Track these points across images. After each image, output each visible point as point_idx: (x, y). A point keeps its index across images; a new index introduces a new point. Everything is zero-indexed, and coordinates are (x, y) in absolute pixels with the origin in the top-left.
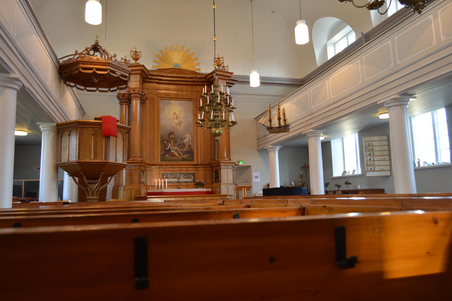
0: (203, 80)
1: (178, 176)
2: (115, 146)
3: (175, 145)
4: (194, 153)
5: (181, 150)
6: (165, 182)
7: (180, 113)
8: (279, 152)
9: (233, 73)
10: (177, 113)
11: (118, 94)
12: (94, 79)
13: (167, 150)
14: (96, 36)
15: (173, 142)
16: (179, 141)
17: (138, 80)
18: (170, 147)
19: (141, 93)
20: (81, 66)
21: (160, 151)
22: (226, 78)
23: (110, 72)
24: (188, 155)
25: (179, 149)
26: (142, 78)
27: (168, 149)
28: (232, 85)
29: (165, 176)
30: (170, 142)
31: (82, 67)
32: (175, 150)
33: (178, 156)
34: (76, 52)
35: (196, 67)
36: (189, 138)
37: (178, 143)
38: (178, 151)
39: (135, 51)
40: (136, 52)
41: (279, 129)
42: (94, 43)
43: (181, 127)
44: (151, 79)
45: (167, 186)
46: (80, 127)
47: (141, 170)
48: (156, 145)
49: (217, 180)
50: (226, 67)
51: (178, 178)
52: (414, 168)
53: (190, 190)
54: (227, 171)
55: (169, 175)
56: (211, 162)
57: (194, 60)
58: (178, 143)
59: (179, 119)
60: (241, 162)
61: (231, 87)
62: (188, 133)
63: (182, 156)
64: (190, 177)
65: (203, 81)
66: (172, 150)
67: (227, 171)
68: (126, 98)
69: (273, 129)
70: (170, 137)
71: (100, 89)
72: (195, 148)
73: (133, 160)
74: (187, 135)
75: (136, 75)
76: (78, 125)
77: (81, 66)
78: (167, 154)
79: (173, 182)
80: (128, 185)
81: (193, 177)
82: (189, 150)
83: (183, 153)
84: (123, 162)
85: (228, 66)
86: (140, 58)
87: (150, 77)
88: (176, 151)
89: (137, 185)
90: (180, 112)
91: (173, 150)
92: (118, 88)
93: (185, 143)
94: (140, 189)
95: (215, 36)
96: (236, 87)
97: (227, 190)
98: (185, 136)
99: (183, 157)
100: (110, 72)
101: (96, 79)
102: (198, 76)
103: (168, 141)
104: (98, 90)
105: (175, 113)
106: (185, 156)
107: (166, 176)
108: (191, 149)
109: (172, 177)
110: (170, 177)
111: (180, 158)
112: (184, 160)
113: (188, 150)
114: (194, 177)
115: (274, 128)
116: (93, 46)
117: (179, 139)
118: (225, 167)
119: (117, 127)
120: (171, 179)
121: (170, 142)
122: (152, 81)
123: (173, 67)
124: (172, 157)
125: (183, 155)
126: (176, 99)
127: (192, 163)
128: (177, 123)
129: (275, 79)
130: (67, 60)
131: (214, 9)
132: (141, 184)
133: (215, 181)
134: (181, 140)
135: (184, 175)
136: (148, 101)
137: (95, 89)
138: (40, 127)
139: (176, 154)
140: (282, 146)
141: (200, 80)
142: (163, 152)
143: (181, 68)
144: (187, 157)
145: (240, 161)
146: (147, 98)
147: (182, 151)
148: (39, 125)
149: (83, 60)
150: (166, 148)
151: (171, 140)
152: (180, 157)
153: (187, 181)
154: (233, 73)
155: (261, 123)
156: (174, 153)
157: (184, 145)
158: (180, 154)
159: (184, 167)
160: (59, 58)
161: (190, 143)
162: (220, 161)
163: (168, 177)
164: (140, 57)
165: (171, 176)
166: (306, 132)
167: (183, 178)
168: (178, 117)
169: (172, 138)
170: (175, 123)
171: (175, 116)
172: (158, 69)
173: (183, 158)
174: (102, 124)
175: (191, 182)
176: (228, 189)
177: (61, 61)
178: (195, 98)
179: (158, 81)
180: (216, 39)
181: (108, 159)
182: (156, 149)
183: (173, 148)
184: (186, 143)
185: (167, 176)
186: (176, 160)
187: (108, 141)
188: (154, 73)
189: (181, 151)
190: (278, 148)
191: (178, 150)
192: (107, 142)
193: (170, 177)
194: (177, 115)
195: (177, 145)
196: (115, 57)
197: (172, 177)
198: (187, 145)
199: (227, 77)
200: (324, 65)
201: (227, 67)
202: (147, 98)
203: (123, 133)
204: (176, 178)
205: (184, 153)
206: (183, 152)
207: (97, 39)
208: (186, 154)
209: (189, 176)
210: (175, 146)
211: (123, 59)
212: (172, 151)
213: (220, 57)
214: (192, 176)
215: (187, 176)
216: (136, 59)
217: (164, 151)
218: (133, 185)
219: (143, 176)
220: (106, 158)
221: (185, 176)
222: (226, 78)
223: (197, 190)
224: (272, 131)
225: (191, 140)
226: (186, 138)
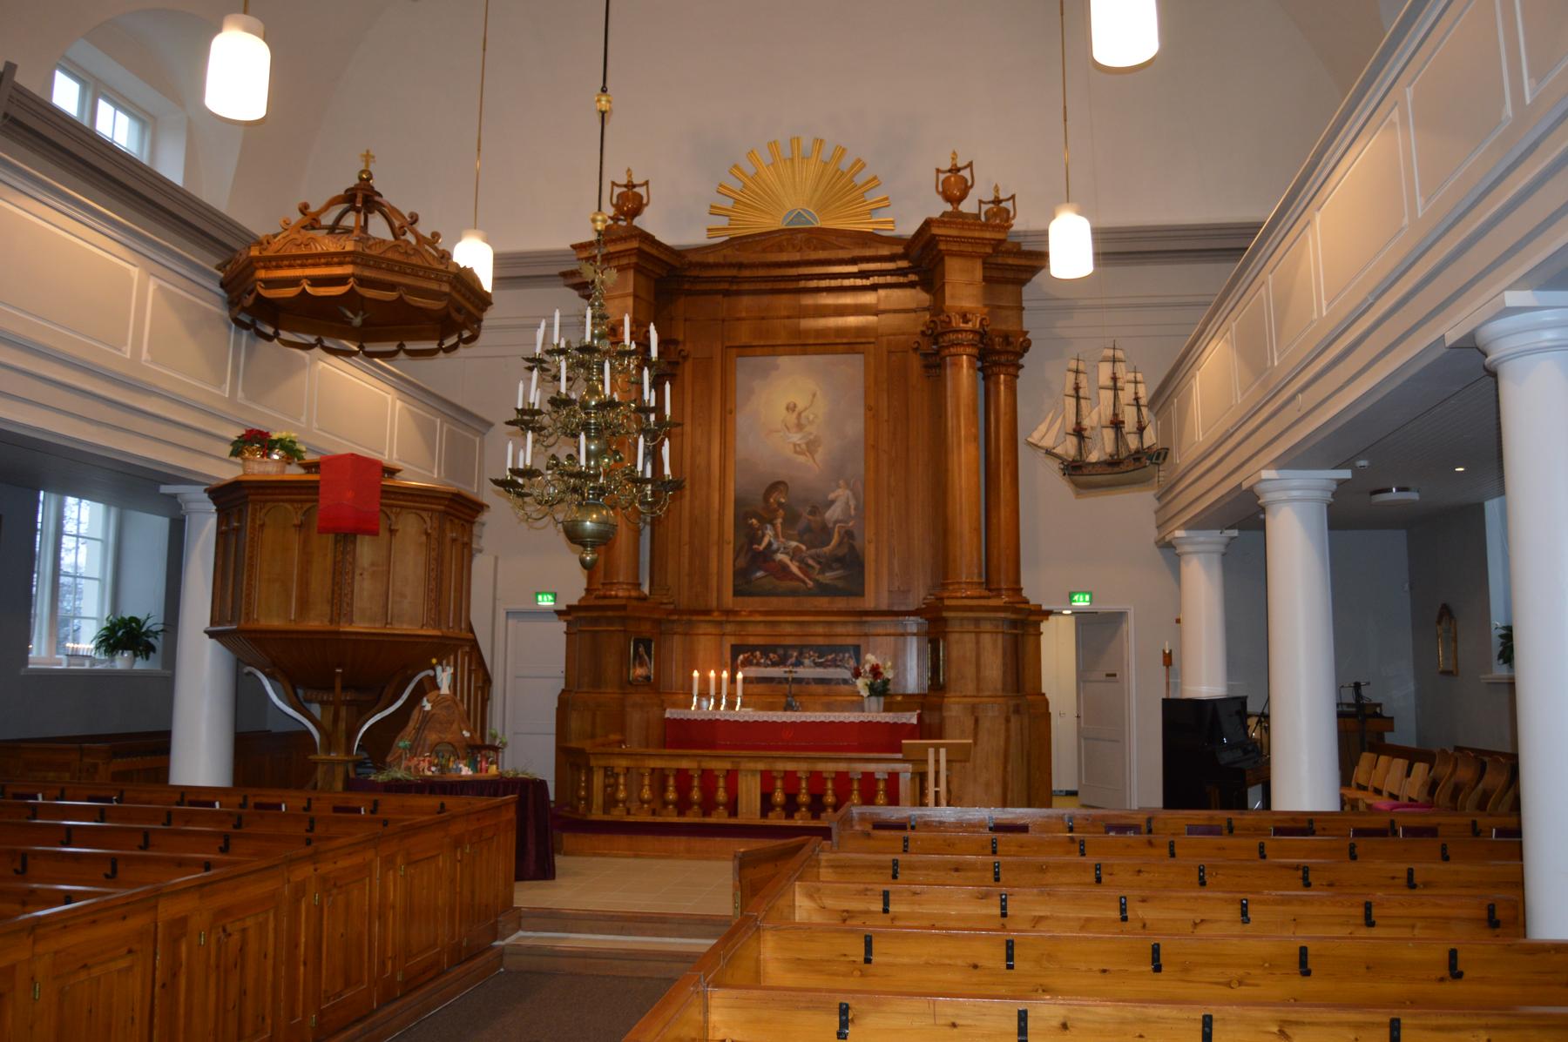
1: (791, 657)
3: (791, 532)
5: (813, 551)
6: (733, 680)
7: (811, 405)
10: (800, 406)
13: (760, 552)
15: (784, 519)
16: (805, 514)
17: (630, 289)
18: (772, 539)
20: (262, 274)
23: (355, 286)
25: (804, 547)
27: (761, 548)
29: (741, 657)
30: (771, 522)
31: (310, 276)
32: (791, 553)
33: (801, 575)
36: (847, 503)
37: (802, 524)
38: (804, 555)
41: (1110, 470)
42: (353, 181)
43: (814, 459)
50: (1008, 200)
53: (811, 717)
54: (978, 642)
55: (758, 653)
57: (863, 189)
58: (802, 524)
59: (808, 429)
60: (1081, 596)
62: (841, 482)
63: (819, 574)
64: (840, 661)
65: (899, 269)
66: (777, 551)
67: (978, 642)
69: (1085, 471)
70: (772, 500)
71: (410, 346)
72: (869, 542)
74: (839, 492)
77: (262, 274)
78: (760, 569)
80: (585, 689)
82: (844, 550)
83: (819, 563)
87: (695, 273)
88: (795, 555)
89: (614, 693)
90: (812, 402)
91: (781, 553)
92: (401, 347)
93: (831, 525)
97: (973, 722)
98: (832, 496)
99: (820, 578)
100: (355, 286)
101: (356, 315)
105: (792, 406)
106: (828, 577)
107: (746, 655)
108: (852, 547)
109: (771, 660)
110: (762, 658)
111: (810, 584)
112: (824, 590)
115: (1090, 468)
117: (808, 509)
119: (383, 491)
120: (766, 666)
121: (771, 522)
122: (699, 287)
123: (783, 227)
124: (778, 578)
125: (822, 571)
126: (799, 348)
128: (799, 445)
134: (815, 511)
135: (815, 652)
139: (794, 568)
142: (742, 562)
143: (816, 225)
144: (839, 578)
146: (683, 353)
147: (818, 556)
149: (265, 254)
150: (755, 546)
152: (810, 579)
153: (829, 677)
155: (1040, 444)
157: (825, 531)
158: (808, 565)
161: (851, 524)
163: (755, 661)
165: (768, 657)
166: (1255, 481)
167: (812, 664)
168: (803, 421)
169: (780, 505)
170: (791, 446)
171: (792, 418)
172: (727, 238)
173: (821, 583)
174: (318, 487)
176: (977, 721)
183: (782, 542)
184: (836, 522)
186: (793, 593)
188: (711, 259)
189: (812, 557)
191: (801, 550)
193: (762, 661)
194: (800, 414)
195: (796, 532)
196: (412, 224)
197: (771, 660)
198: (839, 532)
200: (147, 172)
205: (827, 564)
207: (367, 165)
208: (833, 569)
209: (838, 658)
210: (790, 538)
212: (780, 556)
215: (830, 657)
218: (600, 693)
221: (819, 657)
223: (829, 717)
225: (853, 512)
226: (832, 502)
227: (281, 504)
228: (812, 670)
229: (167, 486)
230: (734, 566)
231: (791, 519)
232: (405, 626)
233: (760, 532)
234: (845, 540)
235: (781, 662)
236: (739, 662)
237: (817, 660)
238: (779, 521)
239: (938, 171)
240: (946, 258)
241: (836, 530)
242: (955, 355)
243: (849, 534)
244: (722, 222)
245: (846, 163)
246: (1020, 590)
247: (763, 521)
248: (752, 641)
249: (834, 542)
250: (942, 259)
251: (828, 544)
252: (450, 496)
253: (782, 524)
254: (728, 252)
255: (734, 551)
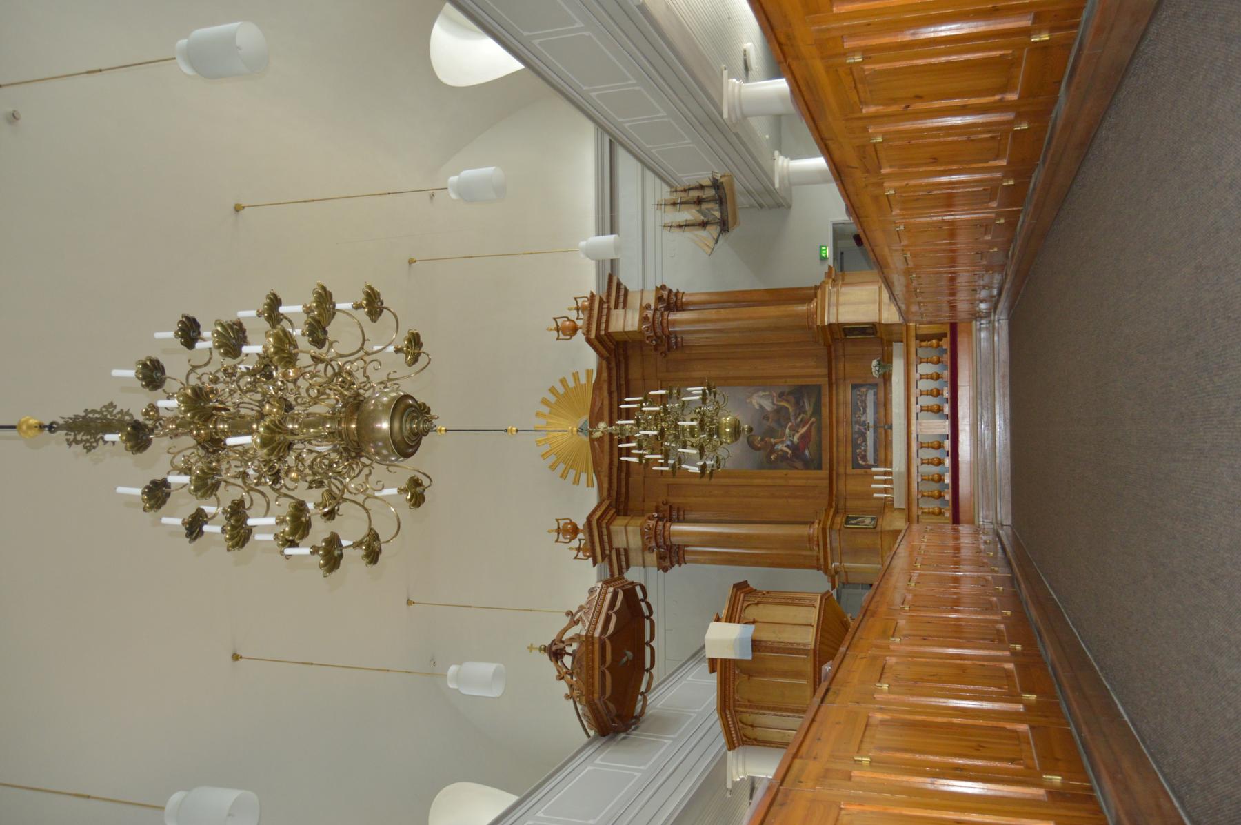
0: (613, 364)
2: (777, 625)
4: (799, 384)
5: (792, 418)
8: (793, 158)
9: (592, 292)
11: (658, 570)
12: (625, 659)
14: (531, 651)
15: (771, 437)
18: (785, 445)
19: (653, 522)
21: (796, 471)
22: (605, 312)
24: (805, 400)
25: (790, 424)
26: (618, 517)
28: (622, 287)
29: (860, 462)
30: (773, 446)
34: (567, 697)
35: (583, 380)
37: (774, 425)
39: (556, 534)
40: (558, 531)
42: (546, 657)
44: (618, 493)
45: (885, 467)
46: (734, 706)
47: (842, 527)
48: (781, 482)
49: (871, 331)
51: (865, 429)
52: (726, 622)
55: (858, 451)
56: (821, 342)
58: (774, 425)
61: (628, 288)
62: (748, 401)
63: (807, 414)
65: (617, 366)
66: (792, 441)
68: (668, 552)
69: (726, 218)
70: (759, 445)
71: (647, 638)
73: (818, 545)
74: (754, 402)
75: (612, 534)
76: (729, 709)
78: (804, 454)
79: (874, 440)
81: (863, 390)
83: (799, 414)
84: (815, 607)
85: (575, 299)
86: (570, 520)
88: (794, 430)
93: (775, 407)
94: (891, 531)
95: (507, 431)
96: (630, 278)
98: (757, 407)
99: (809, 414)
101: (625, 655)
102: (605, 375)
103: (769, 450)
104: (651, 644)
106: (808, 408)
107: (859, 459)
108: (790, 393)
111: (813, 419)
112: (817, 411)
113: (793, 400)
114: (862, 385)
116: (552, 658)
117: (765, 422)
118: (833, 310)
120: (866, 445)
121: (773, 446)
122: (623, 490)
124: (810, 441)
125: (805, 412)
127: (825, 390)
129: (600, 216)
130: (587, 721)
131: (446, 431)
132: (879, 529)
133: (873, 334)
134: (766, 418)
136: (674, 500)
137: (648, 650)
138: (738, 779)
139: (803, 430)
140: (777, 153)
141: (614, 372)
142: (799, 464)
144: (809, 401)
145: (821, 256)
146: (665, 502)
147: (795, 414)
148: (733, 781)
150: (789, 456)
151: (766, 442)
154: (592, 292)
156: (800, 436)
157: (779, 411)
159: (837, 413)
160: (586, 739)
161: (774, 394)
162: (818, 326)
163: (863, 453)
164: (568, 521)
165: (860, 444)
169: (762, 440)
172: (594, 475)
175: (876, 394)
177: (592, 733)
178: (659, 383)
179: (623, 475)
180: (514, 429)
181: (807, 648)
182: (791, 482)
184: (774, 404)
185: (858, 455)
186: (819, 431)
187: (763, 644)
188: (606, 485)
189: (796, 418)
190: (780, 162)
191: (791, 427)
192: (766, 647)
193: (863, 448)
197: (862, 442)
198: (781, 401)
199: (602, 308)
201: (578, 300)
202: (665, 502)
203: (746, 604)
204: (866, 433)
205: (800, 409)
206: (798, 412)
207: (536, 648)
208: (803, 406)
209: (860, 399)
210: (784, 434)
211: (577, 555)
212: (796, 439)
213: (556, 527)
214: (859, 391)
215: (860, 404)
216: (575, 531)
217: (794, 462)
219: (859, 520)
220: (805, 652)
222: (605, 312)
224: (730, 219)
225: (767, 393)
226: (761, 406)
227: (735, 687)
228: (868, 416)
229: (727, 784)
230: (802, 469)
231: (771, 432)
232: (814, 616)
233: (780, 453)
234: (784, 397)
235: (864, 435)
236: (864, 463)
237: (862, 412)
238: (772, 440)
239: (558, 339)
240: (610, 331)
241: (778, 403)
242: (668, 324)
243: (781, 395)
244: (584, 477)
245: (552, 399)
246: (816, 286)
247: (772, 451)
248: (850, 455)
249: (786, 404)
250: (609, 333)
251: (787, 408)
252: (735, 589)
253: (775, 439)
254: (602, 475)
255: (790, 469)
